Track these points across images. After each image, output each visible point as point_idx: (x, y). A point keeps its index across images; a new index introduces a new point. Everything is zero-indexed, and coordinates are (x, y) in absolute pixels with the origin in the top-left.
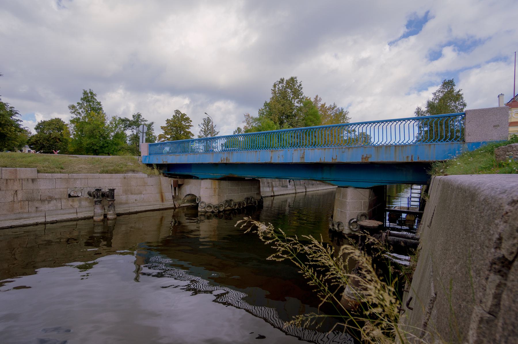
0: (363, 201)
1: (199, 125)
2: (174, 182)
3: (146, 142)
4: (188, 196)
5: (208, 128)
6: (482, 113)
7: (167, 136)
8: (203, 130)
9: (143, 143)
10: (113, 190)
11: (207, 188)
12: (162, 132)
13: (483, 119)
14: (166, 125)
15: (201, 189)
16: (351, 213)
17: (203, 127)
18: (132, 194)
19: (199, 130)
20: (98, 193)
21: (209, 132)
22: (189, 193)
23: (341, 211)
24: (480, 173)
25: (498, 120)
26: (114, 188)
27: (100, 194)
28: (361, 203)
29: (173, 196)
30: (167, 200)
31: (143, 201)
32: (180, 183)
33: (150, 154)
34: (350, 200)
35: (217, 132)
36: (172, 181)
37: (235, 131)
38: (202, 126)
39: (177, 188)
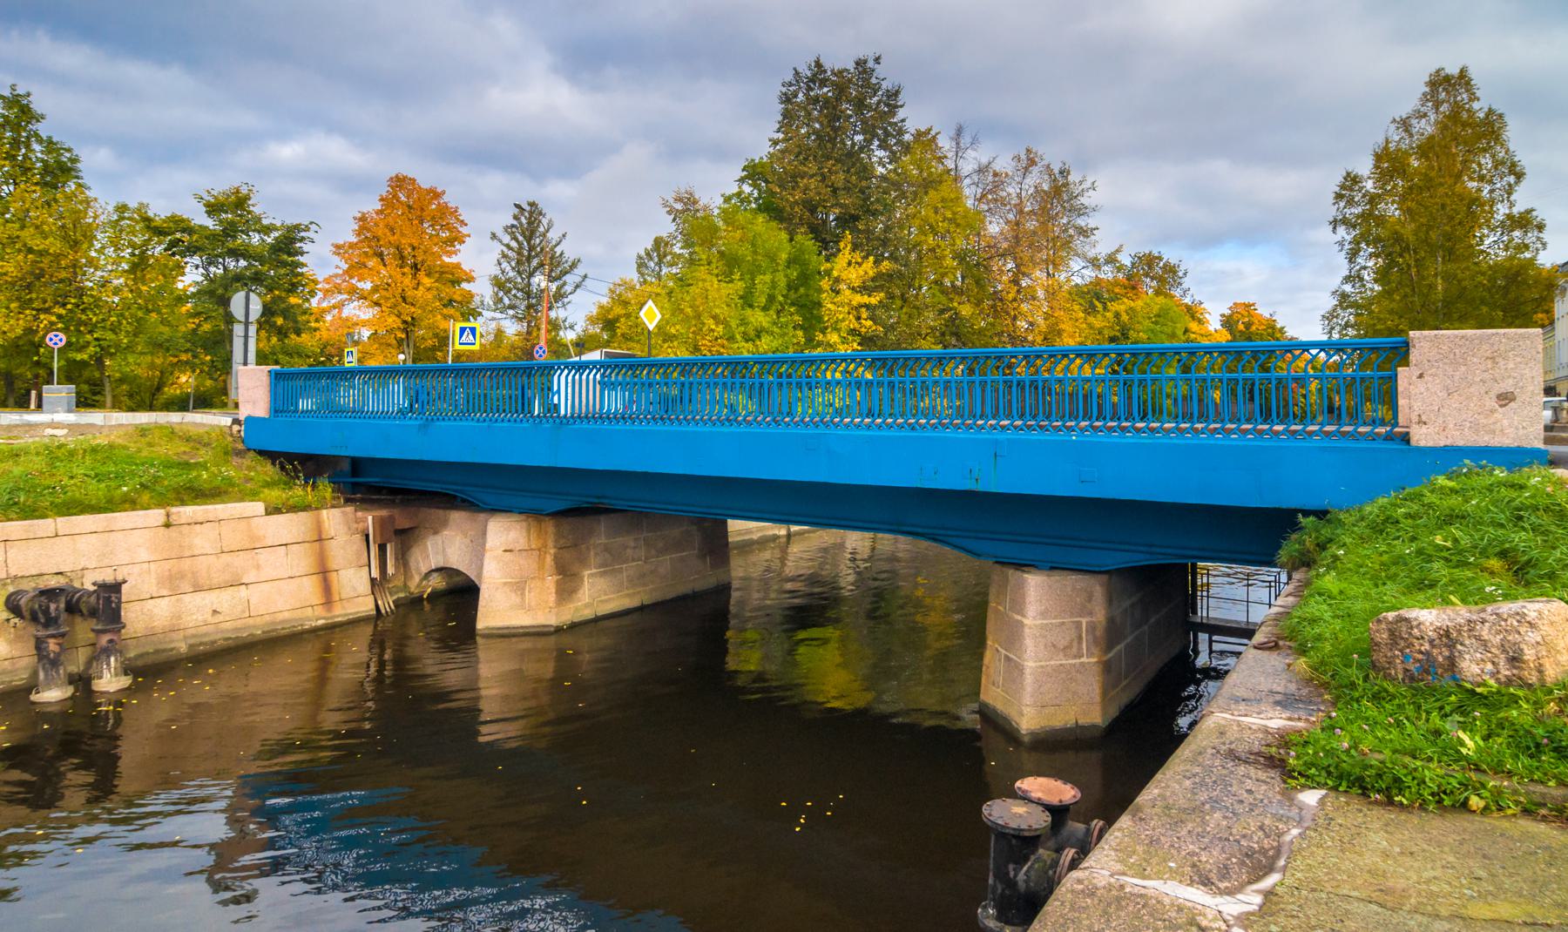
0: (1084, 621)
1: (494, 236)
2: (381, 524)
3: (258, 363)
4: (435, 575)
5: (531, 248)
6: (1461, 346)
7: (360, 285)
8: (510, 253)
9: (245, 364)
10: (115, 588)
11: (511, 551)
12: (339, 265)
13: (1463, 368)
14: (354, 239)
15: (488, 555)
16: (1042, 667)
17: (514, 244)
18: (198, 589)
19: (497, 255)
20: (53, 606)
21: (535, 263)
22: (441, 564)
23: (1008, 658)
24: (1429, 604)
25: (1509, 377)
26: (120, 578)
27: (57, 609)
28: (1079, 625)
29: (373, 580)
30: (348, 599)
31: (244, 612)
32: (403, 523)
33: (276, 411)
34: (1034, 618)
35: (571, 260)
36: (370, 518)
37: (643, 253)
38: (507, 239)
39: (388, 546)
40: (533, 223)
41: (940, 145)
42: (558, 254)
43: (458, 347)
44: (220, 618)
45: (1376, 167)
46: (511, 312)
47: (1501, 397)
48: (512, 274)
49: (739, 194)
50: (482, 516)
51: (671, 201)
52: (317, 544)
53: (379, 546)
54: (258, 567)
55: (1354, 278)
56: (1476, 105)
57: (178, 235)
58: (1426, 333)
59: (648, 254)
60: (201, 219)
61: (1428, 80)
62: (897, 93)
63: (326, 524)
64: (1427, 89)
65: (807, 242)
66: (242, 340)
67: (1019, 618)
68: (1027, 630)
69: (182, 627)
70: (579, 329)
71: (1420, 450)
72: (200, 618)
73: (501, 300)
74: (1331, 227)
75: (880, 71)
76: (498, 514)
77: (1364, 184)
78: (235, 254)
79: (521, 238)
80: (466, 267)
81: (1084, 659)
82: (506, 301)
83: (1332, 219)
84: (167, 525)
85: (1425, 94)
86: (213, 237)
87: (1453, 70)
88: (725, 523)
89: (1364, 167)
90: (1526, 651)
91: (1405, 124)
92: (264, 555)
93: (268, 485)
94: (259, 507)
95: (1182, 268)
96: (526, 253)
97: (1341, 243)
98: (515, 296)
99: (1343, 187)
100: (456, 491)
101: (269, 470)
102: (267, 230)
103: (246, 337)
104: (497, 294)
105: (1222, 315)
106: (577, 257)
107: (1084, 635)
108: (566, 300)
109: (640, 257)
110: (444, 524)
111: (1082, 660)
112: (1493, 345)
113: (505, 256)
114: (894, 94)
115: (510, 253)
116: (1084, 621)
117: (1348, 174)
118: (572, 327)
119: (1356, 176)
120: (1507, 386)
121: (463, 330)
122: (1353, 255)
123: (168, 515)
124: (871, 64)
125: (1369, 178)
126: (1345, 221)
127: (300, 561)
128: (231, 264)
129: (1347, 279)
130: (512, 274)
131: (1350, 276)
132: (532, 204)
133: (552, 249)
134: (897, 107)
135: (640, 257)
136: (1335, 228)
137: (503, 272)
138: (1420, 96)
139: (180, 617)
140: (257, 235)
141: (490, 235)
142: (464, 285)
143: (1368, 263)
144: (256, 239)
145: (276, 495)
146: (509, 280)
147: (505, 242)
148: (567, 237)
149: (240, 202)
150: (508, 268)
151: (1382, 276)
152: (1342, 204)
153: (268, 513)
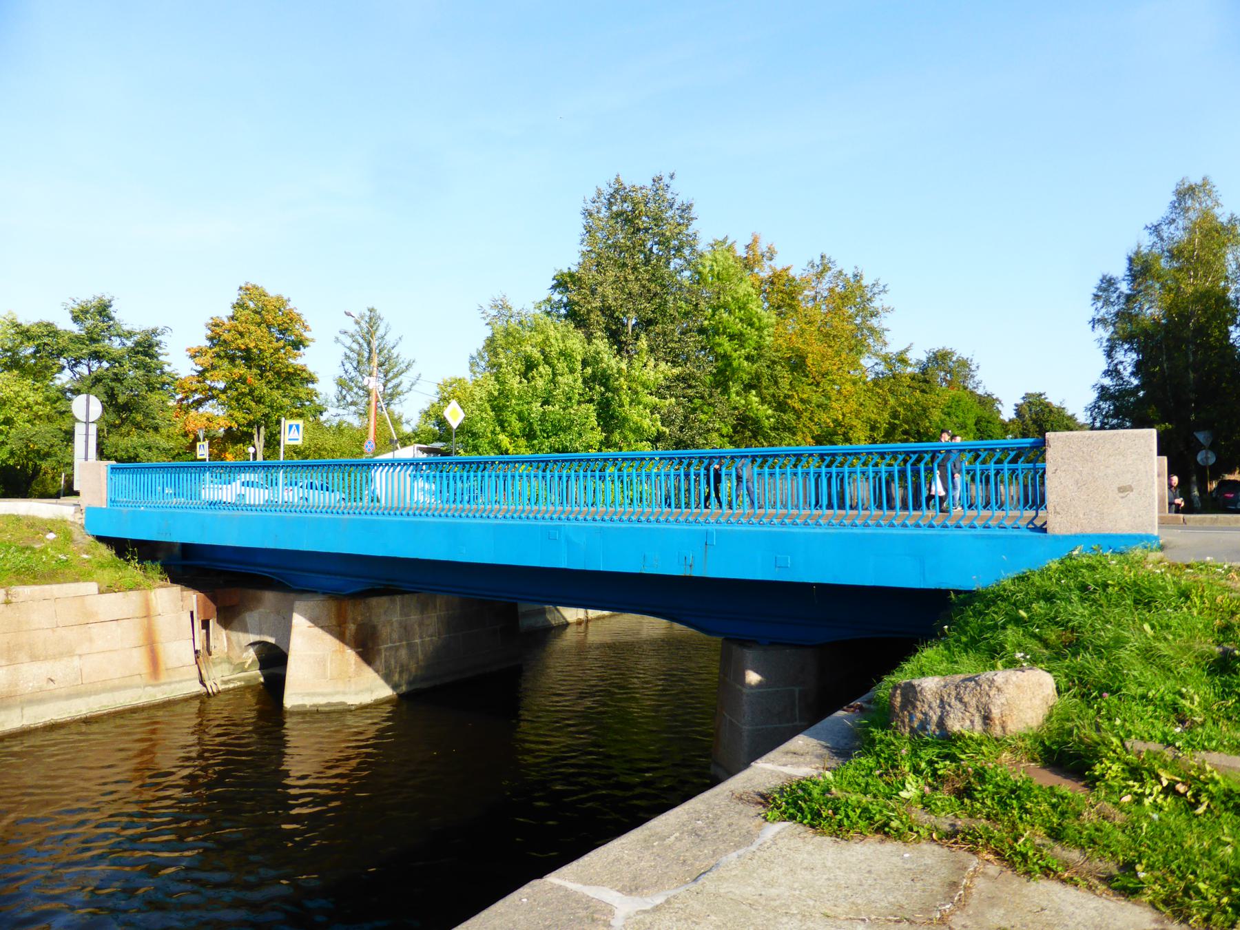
0: (797, 689)
8: (353, 355)
17: (355, 346)
18: (34, 658)
30: (174, 669)
31: (77, 679)
37: (475, 354)
39: (211, 622)
40: (372, 327)
41: (1199, 182)
42: (395, 356)
43: (288, 442)
44: (51, 686)
45: (1130, 270)
46: (353, 408)
47: (1122, 490)
48: (353, 374)
49: (549, 300)
50: (292, 596)
51: (487, 308)
52: (145, 620)
53: (203, 621)
54: (91, 640)
55: (1113, 372)
56: (1217, 211)
57: (46, 340)
58: (1059, 434)
59: (479, 354)
60: (66, 324)
61: (1174, 189)
62: (689, 207)
63: (154, 602)
64: (1175, 198)
65: (601, 344)
66: (84, 437)
67: (739, 687)
68: (745, 698)
69: (19, 693)
70: (414, 424)
71: (1056, 538)
72: (36, 685)
73: (344, 397)
74: (1091, 325)
75: (675, 186)
76: (304, 596)
77: (1118, 286)
78: (97, 356)
79: (361, 341)
80: (310, 369)
81: (796, 723)
82: (349, 399)
83: (1091, 319)
84: (7, 603)
85: (1173, 203)
86: (77, 340)
87: (1195, 179)
88: (516, 604)
89: (1119, 270)
90: (993, 711)
91: (1156, 230)
92: (95, 629)
93: (102, 566)
94: (92, 587)
95: (975, 362)
96: (366, 355)
97: (1100, 340)
98: (356, 393)
99: (1099, 288)
100: (270, 573)
101: (106, 552)
102: (130, 334)
103: (87, 435)
104: (341, 392)
105: (1016, 405)
106: (412, 358)
107: (797, 702)
108: (401, 397)
109: (472, 358)
110: (259, 601)
111: (796, 723)
112: (1114, 444)
113: (347, 357)
114: (686, 209)
115: (353, 355)
116: (797, 689)
117: (1104, 277)
118: (408, 422)
119: (1111, 279)
120: (1126, 480)
121: (291, 426)
122: (1109, 354)
123: (7, 594)
124: (666, 180)
125: (1124, 280)
126: (1103, 321)
127: (130, 634)
128: (95, 365)
129: (1107, 373)
130: (353, 374)
131: (1108, 370)
132: (371, 310)
133: (389, 351)
134: (692, 219)
135: (472, 358)
136: (1093, 327)
137: (346, 372)
138: (1168, 204)
139: (17, 685)
140: (118, 340)
141: (334, 339)
142: (310, 386)
143: (1127, 359)
144: (116, 342)
145: (108, 575)
146: (351, 380)
147: (348, 345)
148: (403, 339)
149: (103, 310)
150: (351, 369)
151: (1139, 368)
152: (1100, 304)
153: (101, 592)
